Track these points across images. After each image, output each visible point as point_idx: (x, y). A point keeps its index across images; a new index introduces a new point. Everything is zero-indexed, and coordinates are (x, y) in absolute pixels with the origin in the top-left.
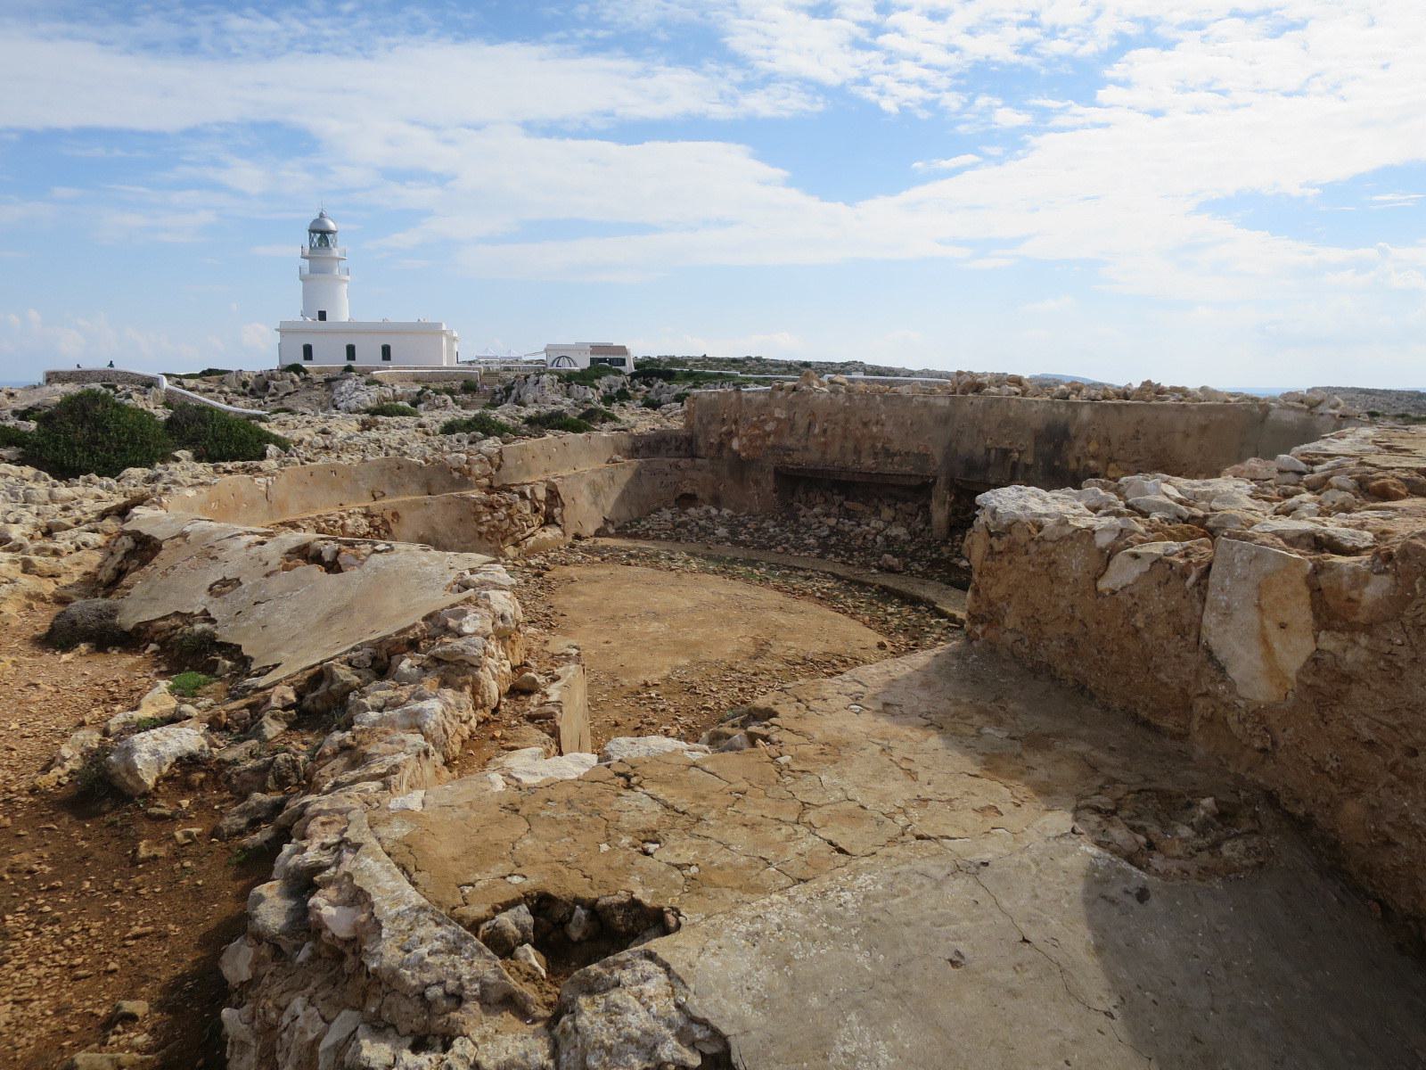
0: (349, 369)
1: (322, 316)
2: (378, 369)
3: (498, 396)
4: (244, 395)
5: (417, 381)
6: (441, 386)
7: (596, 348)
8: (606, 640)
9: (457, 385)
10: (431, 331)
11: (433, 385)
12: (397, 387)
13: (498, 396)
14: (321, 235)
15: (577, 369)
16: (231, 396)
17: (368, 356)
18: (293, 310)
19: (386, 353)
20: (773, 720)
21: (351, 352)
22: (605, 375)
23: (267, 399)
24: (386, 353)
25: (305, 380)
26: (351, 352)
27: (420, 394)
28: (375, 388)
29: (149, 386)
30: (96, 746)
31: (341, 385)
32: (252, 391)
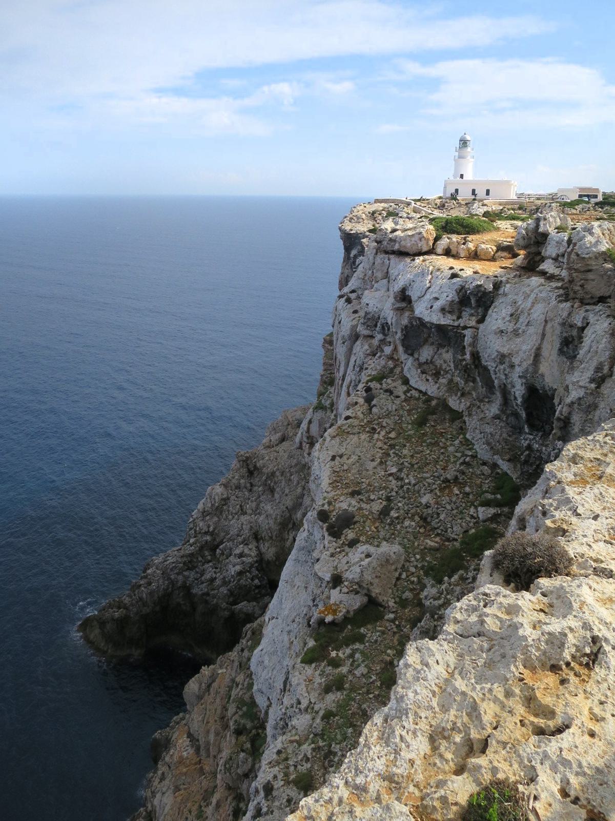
0: (474, 199)
1: (462, 176)
2: (485, 199)
3: (533, 212)
4: (436, 208)
5: (500, 205)
6: (510, 207)
7: (581, 189)
8: (434, 307)
9: (516, 206)
10: (507, 183)
11: (507, 206)
12: (493, 207)
13: (533, 212)
14: (464, 143)
15: (569, 201)
16: (433, 209)
17: (481, 193)
18: (449, 174)
19: (488, 192)
20: (560, 672)
21: (474, 192)
22: (581, 204)
23: (445, 210)
24: (488, 192)
25: (457, 203)
26: (474, 192)
27: (502, 209)
28: (485, 207)
29: (409, 205)
30: (407, 294)
31: (473, 206)
32: (439, 207)
